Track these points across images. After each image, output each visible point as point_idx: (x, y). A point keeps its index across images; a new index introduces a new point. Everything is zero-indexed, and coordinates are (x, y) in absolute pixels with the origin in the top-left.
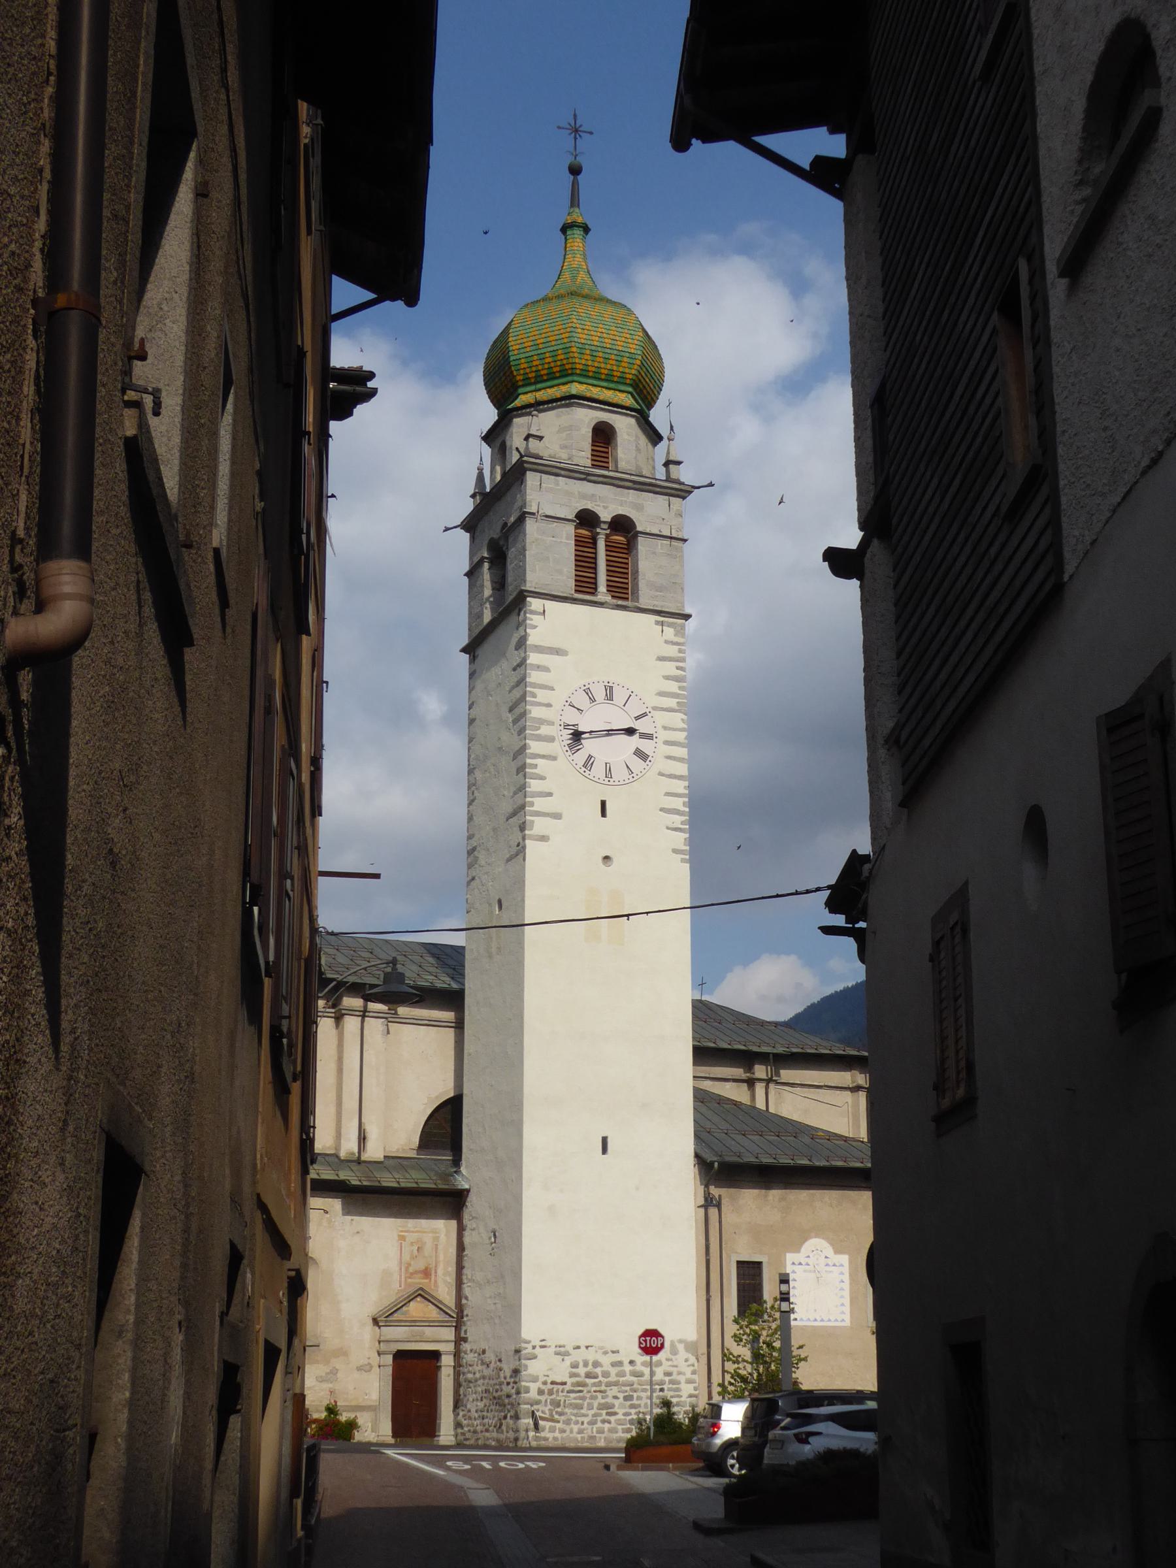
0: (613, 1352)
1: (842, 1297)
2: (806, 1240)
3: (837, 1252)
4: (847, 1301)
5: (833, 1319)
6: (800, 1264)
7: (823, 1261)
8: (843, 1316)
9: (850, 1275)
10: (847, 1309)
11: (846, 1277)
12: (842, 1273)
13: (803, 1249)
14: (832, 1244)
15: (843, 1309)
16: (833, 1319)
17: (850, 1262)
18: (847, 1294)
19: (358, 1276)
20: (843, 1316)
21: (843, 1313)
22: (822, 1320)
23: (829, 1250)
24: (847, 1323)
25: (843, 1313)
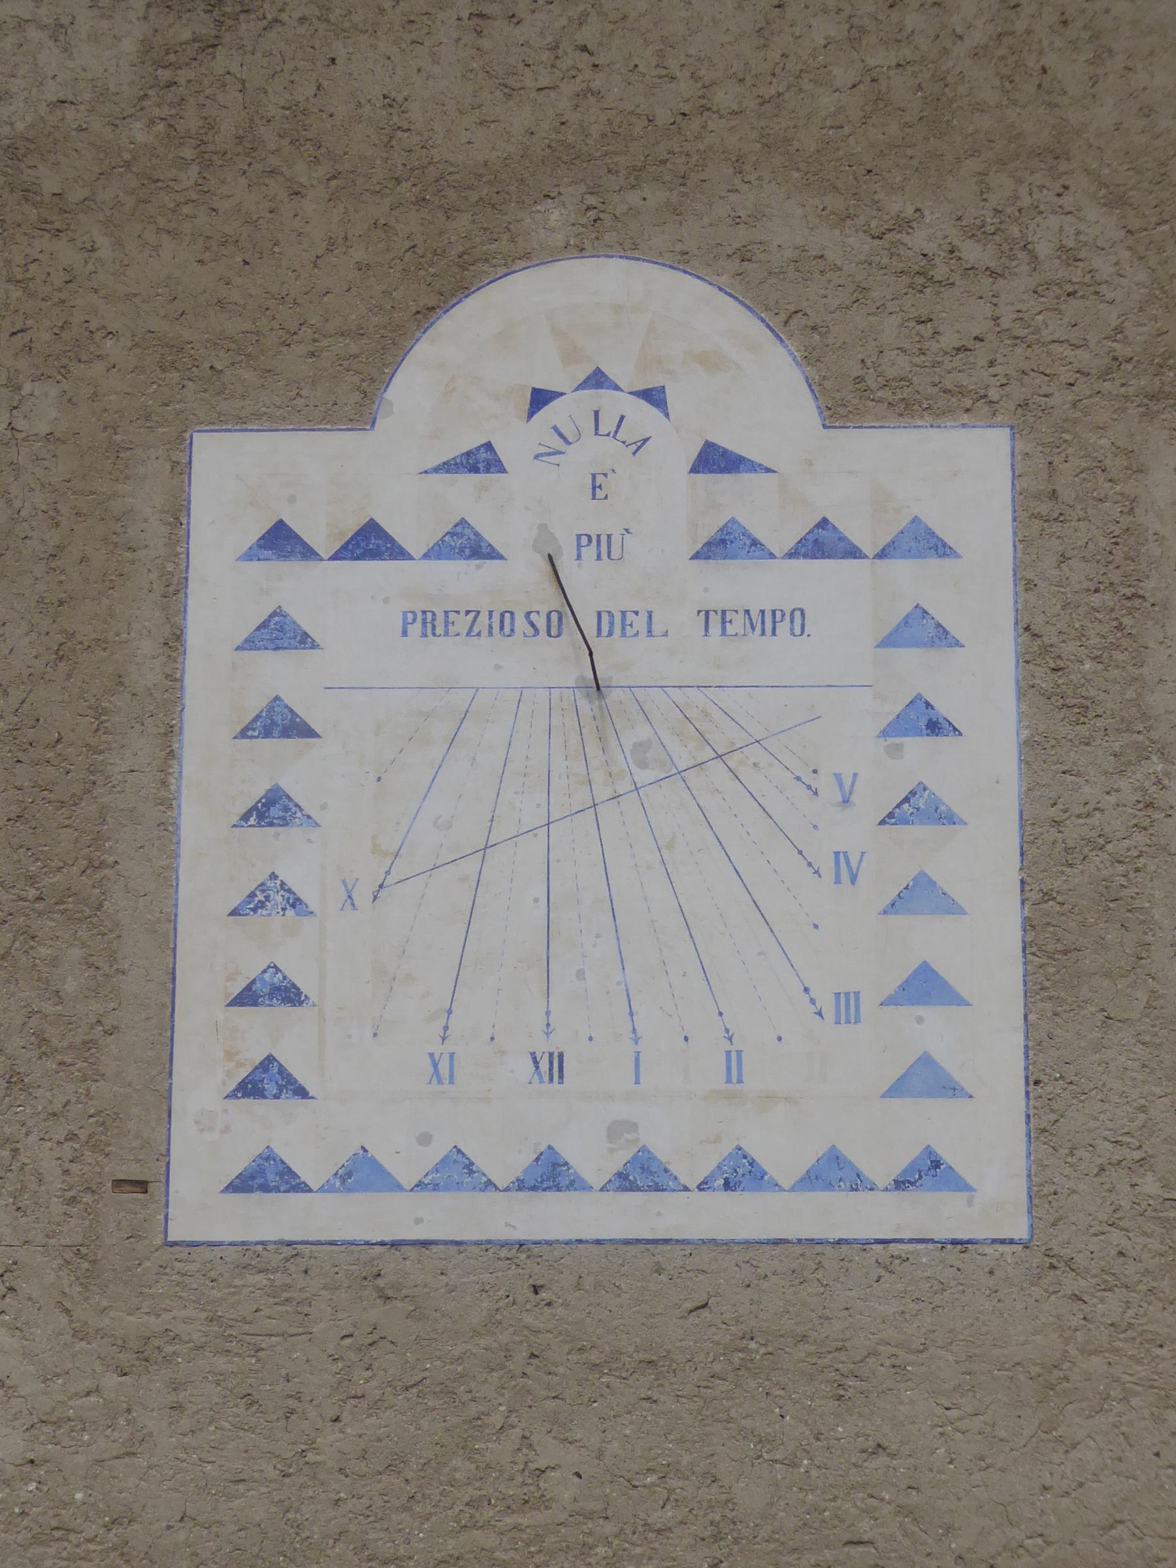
0: (490, 618)
1: (919, 896)
2: (451, 278)
3: (850, 397)
4: (986, 944)
5: (783, 1151)
6: (369, 542)
7: (665, 503)
8: (928, 1125)
9: (1036, 644)
10: (988, 1037)
11: (983, 683)
12: (921, 630)
13: (411, 387)
14: (787, 320)
15: (932, 1031)
16: (784, 1157)
17: (1039, 510)
18: (984, 863)
19: (205, 1140)
20: (928, 1125)
21: (926, 1080)
22: (741, 1175)
23: (760, 388)
24: (993, 1198)
25: (926, 1080)
